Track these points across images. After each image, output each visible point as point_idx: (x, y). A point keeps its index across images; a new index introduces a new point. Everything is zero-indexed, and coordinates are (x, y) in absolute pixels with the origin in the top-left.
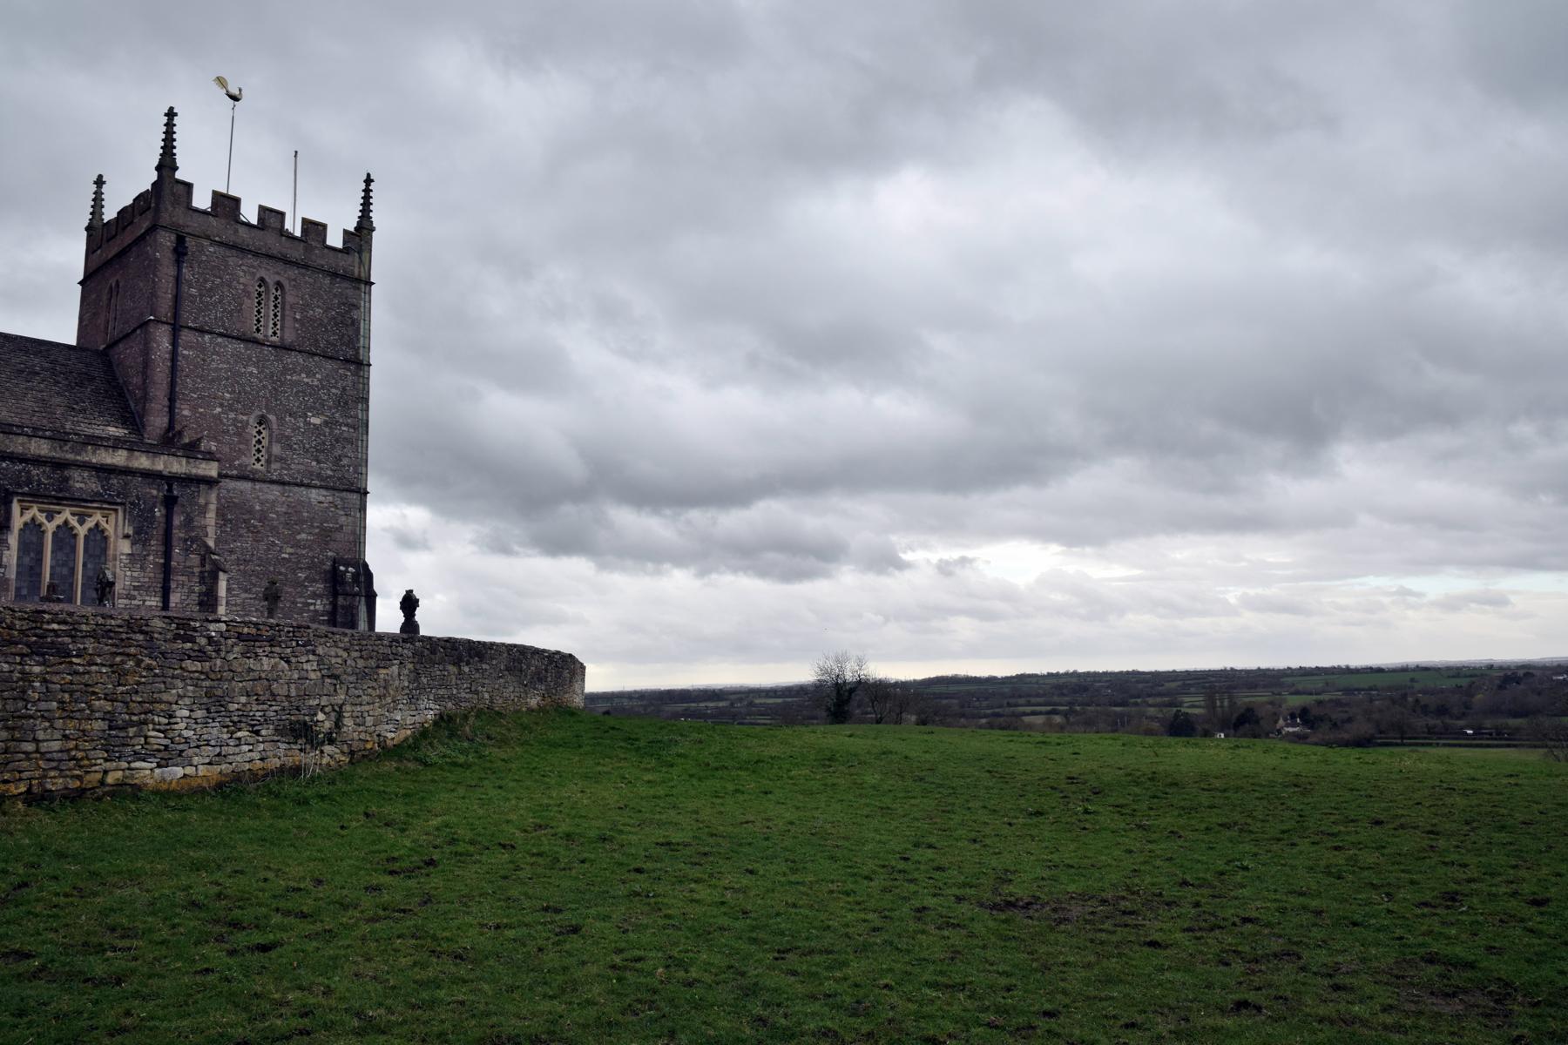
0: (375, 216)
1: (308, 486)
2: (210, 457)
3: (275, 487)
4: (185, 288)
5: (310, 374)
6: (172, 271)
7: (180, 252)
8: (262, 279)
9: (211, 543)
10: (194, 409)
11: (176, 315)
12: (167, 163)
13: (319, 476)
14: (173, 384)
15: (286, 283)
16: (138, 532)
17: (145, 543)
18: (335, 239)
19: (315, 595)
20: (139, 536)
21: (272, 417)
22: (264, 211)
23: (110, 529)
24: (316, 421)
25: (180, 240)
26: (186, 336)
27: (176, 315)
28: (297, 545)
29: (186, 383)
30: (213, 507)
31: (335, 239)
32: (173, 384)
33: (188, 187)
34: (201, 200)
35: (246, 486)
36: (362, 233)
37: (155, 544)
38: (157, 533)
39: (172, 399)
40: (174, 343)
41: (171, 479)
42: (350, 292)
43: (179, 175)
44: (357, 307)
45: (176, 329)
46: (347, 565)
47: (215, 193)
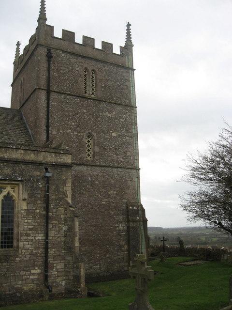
0: (134, 40)
1: (112, 167)
2: (67, 152)
3: (97, 168)
4: (52, 73)
5: (110, 112)
6: (46, 65)
7: (49, 56)
8: (86, 69)
9: (70, 201)
10: (58, 130)
11: (49, 86)
12: (42, 18)
13: (117, 162)
14: (48, 119)
15: (97, 70)
16: (30, 196)
17: (35, 203)
18: (116, 51)
19: (119, 222)
20: (31, 199)
21: (94, 134)
22: (85, 38)
23: (15, 195)
24: (114, 135)
25: (49, 51)
26: (53, 96)
27: (49, 86)
28: (109, 197)
29: (54, 119)
30: (70, 180)
31: (116, 51)
32: (48, 119)
33: (52, 28)
34: (58, 34)
35: (84, 168)
36: (127, 48)
37: (40, 204)
38: (40, 195)
39: (48, 127)
40: (48, 99)
41: (47, 167)
42: (125, 74)
43: (47, 23)
44: (129, 81)
45: (49, 92)
46: (133, 206)
47: (83, 36)
